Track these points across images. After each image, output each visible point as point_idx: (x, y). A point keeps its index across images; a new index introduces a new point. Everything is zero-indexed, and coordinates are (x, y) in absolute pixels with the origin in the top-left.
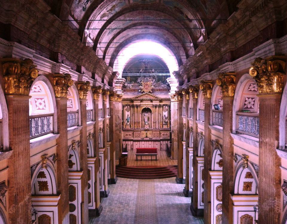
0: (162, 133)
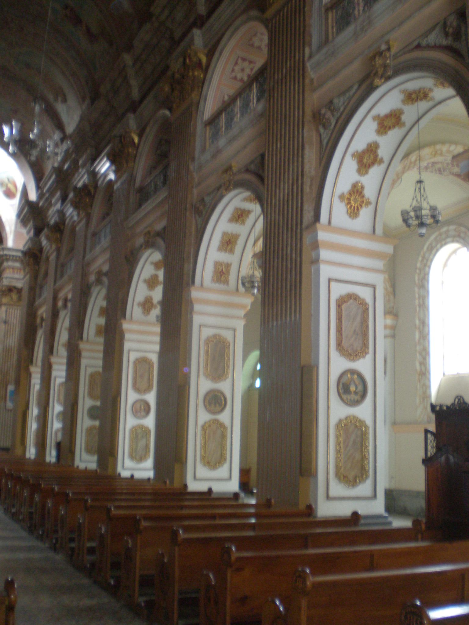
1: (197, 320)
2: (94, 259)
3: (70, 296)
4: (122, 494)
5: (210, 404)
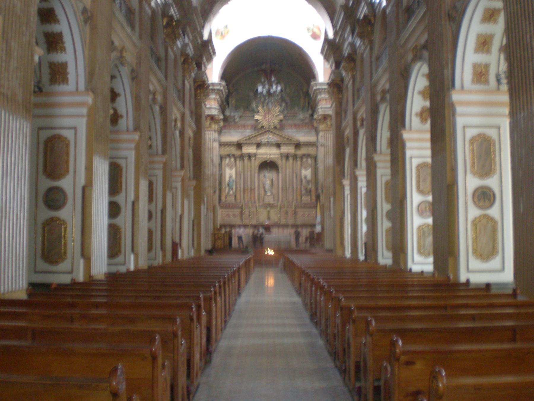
0: (300, 212)
1: (460, 122)
2: (379, 80)
3: (364, 116)
4: (413, 285)
5: (479, 200)
